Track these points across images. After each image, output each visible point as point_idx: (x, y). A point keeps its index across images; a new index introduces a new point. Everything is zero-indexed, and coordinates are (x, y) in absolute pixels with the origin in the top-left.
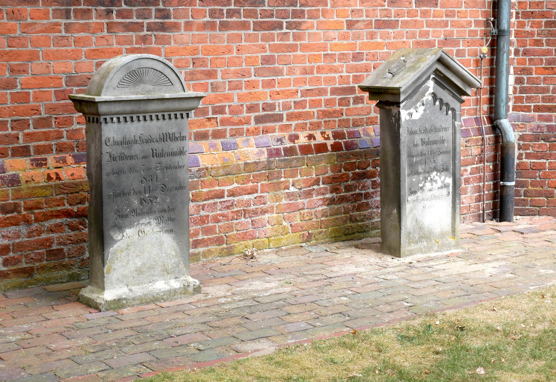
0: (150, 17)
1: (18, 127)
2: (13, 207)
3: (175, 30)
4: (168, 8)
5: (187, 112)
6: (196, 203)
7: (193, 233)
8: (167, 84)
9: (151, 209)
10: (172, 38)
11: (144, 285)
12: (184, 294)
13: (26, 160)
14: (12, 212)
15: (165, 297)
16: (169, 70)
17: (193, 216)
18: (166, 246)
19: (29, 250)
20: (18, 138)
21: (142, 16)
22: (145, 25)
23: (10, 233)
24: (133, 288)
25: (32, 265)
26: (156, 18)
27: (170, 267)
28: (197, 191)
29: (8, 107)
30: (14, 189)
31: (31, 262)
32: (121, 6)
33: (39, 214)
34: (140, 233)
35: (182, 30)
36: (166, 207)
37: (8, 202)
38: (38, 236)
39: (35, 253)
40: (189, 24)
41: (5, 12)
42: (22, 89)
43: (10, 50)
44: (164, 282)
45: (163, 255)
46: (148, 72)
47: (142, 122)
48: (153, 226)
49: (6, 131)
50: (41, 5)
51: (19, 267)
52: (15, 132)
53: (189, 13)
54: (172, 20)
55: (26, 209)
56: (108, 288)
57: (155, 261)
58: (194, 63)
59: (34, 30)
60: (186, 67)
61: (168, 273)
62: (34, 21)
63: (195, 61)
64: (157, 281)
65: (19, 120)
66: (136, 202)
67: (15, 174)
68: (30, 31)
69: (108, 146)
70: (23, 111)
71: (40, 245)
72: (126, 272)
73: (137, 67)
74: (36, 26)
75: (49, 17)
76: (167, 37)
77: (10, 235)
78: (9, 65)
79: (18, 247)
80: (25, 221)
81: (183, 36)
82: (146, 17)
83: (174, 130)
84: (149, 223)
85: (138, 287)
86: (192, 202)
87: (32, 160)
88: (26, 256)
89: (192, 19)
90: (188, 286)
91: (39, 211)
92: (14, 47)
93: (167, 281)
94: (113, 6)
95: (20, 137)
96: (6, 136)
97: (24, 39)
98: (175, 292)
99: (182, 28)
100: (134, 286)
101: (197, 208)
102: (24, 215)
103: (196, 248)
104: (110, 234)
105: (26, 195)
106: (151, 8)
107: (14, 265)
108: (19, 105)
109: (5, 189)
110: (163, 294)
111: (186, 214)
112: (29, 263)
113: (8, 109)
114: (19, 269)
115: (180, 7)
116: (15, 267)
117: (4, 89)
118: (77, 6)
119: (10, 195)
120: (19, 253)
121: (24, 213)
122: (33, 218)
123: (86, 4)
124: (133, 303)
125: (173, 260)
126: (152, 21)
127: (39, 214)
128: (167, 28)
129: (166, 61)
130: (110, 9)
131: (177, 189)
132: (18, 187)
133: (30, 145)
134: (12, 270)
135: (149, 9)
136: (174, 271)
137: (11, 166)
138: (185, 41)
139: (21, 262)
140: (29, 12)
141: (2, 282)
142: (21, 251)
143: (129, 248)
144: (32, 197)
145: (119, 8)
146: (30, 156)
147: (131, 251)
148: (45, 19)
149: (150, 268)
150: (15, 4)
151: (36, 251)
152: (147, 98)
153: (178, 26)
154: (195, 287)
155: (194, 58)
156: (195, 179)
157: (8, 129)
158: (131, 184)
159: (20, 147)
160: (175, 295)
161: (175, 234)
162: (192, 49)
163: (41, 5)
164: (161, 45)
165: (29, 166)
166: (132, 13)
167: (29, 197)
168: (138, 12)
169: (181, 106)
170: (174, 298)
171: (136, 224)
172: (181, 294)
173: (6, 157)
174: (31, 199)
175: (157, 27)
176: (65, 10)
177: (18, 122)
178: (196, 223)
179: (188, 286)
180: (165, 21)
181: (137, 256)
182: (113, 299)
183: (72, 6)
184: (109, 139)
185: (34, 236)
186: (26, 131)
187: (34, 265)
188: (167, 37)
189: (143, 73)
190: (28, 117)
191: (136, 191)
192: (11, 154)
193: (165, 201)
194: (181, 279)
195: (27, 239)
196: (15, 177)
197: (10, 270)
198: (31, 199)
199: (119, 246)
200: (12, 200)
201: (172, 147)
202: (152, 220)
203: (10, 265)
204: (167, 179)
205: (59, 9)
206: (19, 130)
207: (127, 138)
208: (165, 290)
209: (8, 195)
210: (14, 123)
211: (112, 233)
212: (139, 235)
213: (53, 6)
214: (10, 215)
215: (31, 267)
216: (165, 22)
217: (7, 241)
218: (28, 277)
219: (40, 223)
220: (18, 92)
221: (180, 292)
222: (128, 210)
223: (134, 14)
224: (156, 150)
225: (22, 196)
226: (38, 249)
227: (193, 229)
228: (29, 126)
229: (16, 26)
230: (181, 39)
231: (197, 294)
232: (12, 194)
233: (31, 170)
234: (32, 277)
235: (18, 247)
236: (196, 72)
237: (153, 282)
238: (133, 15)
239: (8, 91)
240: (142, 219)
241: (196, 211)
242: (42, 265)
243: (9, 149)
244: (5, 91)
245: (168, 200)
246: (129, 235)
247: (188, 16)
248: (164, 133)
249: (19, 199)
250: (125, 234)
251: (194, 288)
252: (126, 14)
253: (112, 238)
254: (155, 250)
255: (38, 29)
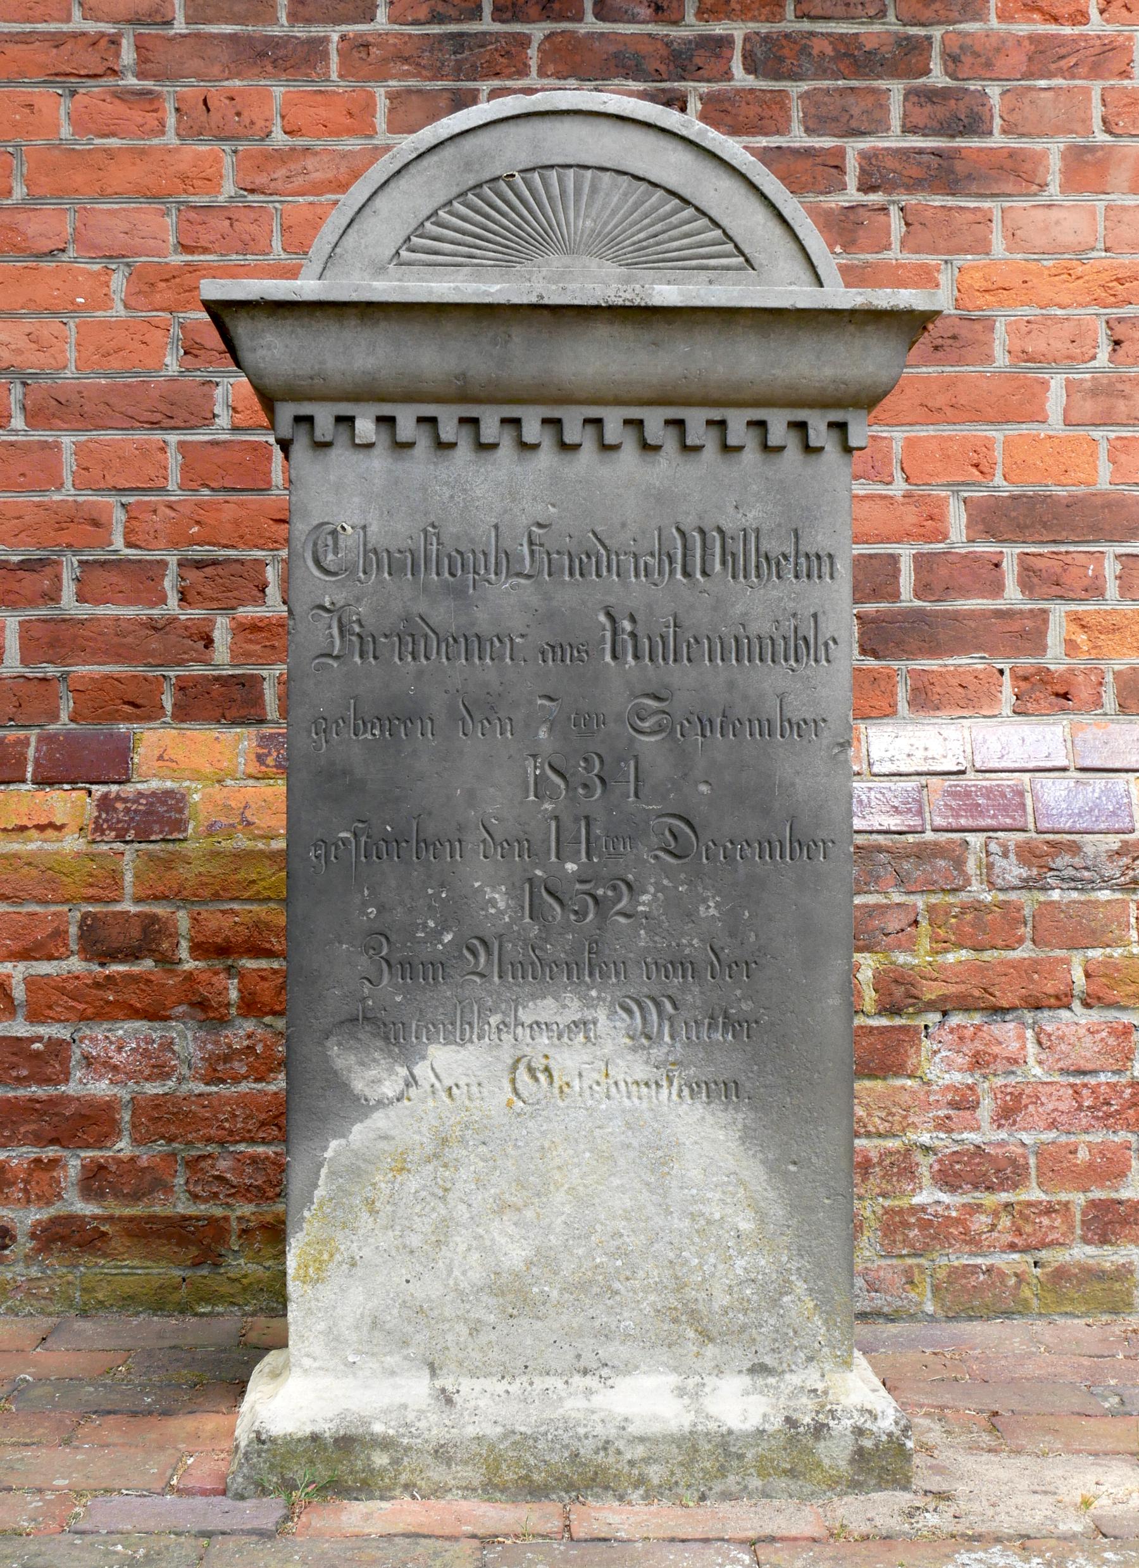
0: (878, 126)
1: (208, 591)
2: (135, 932)
3: (1008, 188)
4: (973, 86)
5: (836, 416)
6: (1111, 1015)
7: (1091, 1165)
8: (713, 262)
9: (595, 946)
10: (997, 225)
11: (540, 1383)
12: (791, 1473)
13: (239, 739)
14: (133, 955)
15: (655, 1473)
16: (727, 184)
17: (1092, 1081)
18: (695, 1174)
19: (209, 1140)
20: (209, 642)
21: (836, 119)
22: (852, 165)
23: (120, 1049)
24: (469, 1389)
25: (218, 1212)
26: (909, 129)
27: (722, 1299)
28: (1117, 953)
29: (170, 506)
30: (151, 856)
31: (215, 1195)
32: (728, 75)
33: (263, 978)
34: (522, 1075)
35: (1054, 188)
36: (693, 945)
37: (118, 908)
38: (257, 1080)
39: (239, 1158)
40: (1088, 157)
41: (169, 106)
42: (235, 429)
43: (188, 264)
44: (673, 1379)
45: (676, 1223)
46: (594, 190)
47: (546, 458)
48: (608, 1048)
49: (153, 605)
50: (334, 76)
51: (157, 1209)
52: (197, 613)
53: (1088, 108)
54: (997, 141)
55: (199, 949)
56: (307, 1362)
57: (621, 1252)
58: (1117, 343)
59: (299, 181)
60: (1070, 357)
61: (706, 1336)
62: (300, 142)
63: (1121, 331)
64: (628, 1369)
65: (215, 563)
66: (500, 898)
67: (169, 793)
68: (279, 185)
69: (327, 572)
70: (237, 523)
71: (263, 1124)
72: (428, 1289)
73: (526, 162)
74: (310, 163)
75: (373, 126)
76: (970, 217)
77: (118, 1059)
78: (182, 326)
79: (154, 1119)
80: (192, 1005)
81: (1054, 214)
82: (854, 124)
83: (753, 516)
84: (582, 1024)
85: (501, 1387)
86: (1087, 1005)
87: (265, 741)
88: (192, 1164)
89: (1108, 137)
90: (819, 1430)
91: (263, 964)
92: (206, 250)
93: (691, 1382)
94: (684, 79)
95: (216, 635)
96: (153, 626)
97: (252, 215)
98: (727, 1454)
99: (1054, 181)
100: (473, 1375)
101: (1112, 1041)
102: (189, 977)
103: (1104, 1241)
104: (327, 1059)
105: (204, 885)
106: (882, 84)
107: (136, 1197)
108: (221, 497)
109: (104, 847)
110: (640, 1451)
111: (834, 1001)
112: (206, 1200)
113: (168, 511)
114: (152, 1219)
115: (1042, 83)
116: (137, 1210)
117: (155, 425)
118: (510, 77)
119: (129, 878)
120: (161, 1147)
121: (190, 965)
122: (234, 995)
123: (551, 69)
124: (438, 1473)
125: (740, 1263)
126: (886, 144)
127: (263, 978)
128: (969, 177)
129: (701, 132)
130: (673, 90)
131: (767, 846)
132: (170, 846)
133: (265, 673)
134: (120, 1219)
135: (874, 91)
136: (743, 1329)
137: (160, 758)
138: (1069, 239)
139: (168, 1189)
140: (277, 104)
141: (76, 1266)
142: (170, 1140)
143: (450, 1154)
144: (234, 899)
145: (715, 86)
146: (262, 721)
147: (463, 1173)
148: (351, 132)
149: (583, 1286)
150: (216, 70)
151: (242, 1147)
152: (533, 299)
153: (1028, 166)
154: (868, 1444)
155: (1120, 320)
156: (1105, 895)
157: (163, 600)
158: (471, 797)
159: (217, 679)
160: (723, 1471)
161: (753, 1108)
162: (1106, 276)
163: (334, 76)
164: (935, 251)
165: (244, 763)
166: (784, 108)
167: (216, 897)
168: (817, 105)
169: (777, 372)
170: (718, 1487)
171: (494, 1020)
172: (763, 1468)
173: (150, 718)
174: (227, 907)
175: (915, 172)
176: (446, 95)
177: (209, 571)
178: (1108, 1116)
179: (819, 1430)
180: (959, 143)
181: (502, 1208)
182: (308, 1430)
183: (486, 76)
184: (334, 533)
185: (237, 1079)
186: (248, 612)
187: (228, 1213)
188: (970, 217)
189: (563, 192)
190: (259, 554)
191: (498, 837)
192: (175, 705)
193: (690, 916)
194: (794, 1379)
195: (201, 1088)
196: (164, 803)
197: (110, 1219)
198: (227, 907)
199: (385, 1138)
200: (138, 900)
201: (739, 609)
202: (601, 1015)
203: (116, 1196)
204: (704, 788)
205: (419, 92)
206: (215, 605)
207: (445, 539)
208: (656, 1429)
209: (115, 877)
210: (193, 575)
211: (341, 1057)
212: (515, 1091)
213: (393, 77)
214: (121, 968)
215: (212, 1220)
216: (958, 150)
217: (104, 1084)
218: (196, 1265)
219: (268, 1019)
220: (214, 443)
221: (760, 1458)
222: (448, 938)
223: (796, 114)
224: (633, 619)
225: (182, 887)
226: (252, 1141)
227: (1089, 1144)
228: (263, 591)
229: (218, 160)
230: (1047, 228)
231: (879, 1488)
232: (136, 876)
233: (251, 782)
234: (217, 1265)
235: (154, 1119)
236: (1127, 388)
237: (605, 1372)
238: (789, 119)
239: (173, 438)
240: (533, 997)
241: (1108, 1052)
242: (269, 1218)
243: (165, 686)
244: (158, 436)
245: (710, 910)
246: (448, 1082)
247: (1086, 121)
248: (689, 522)
249: (166, 898)
250: (421, 1070)
251: (860, 1452)
252: (753, 111)
253: (339, 1086)
254: (622, 1189)
255: (317, 176)
